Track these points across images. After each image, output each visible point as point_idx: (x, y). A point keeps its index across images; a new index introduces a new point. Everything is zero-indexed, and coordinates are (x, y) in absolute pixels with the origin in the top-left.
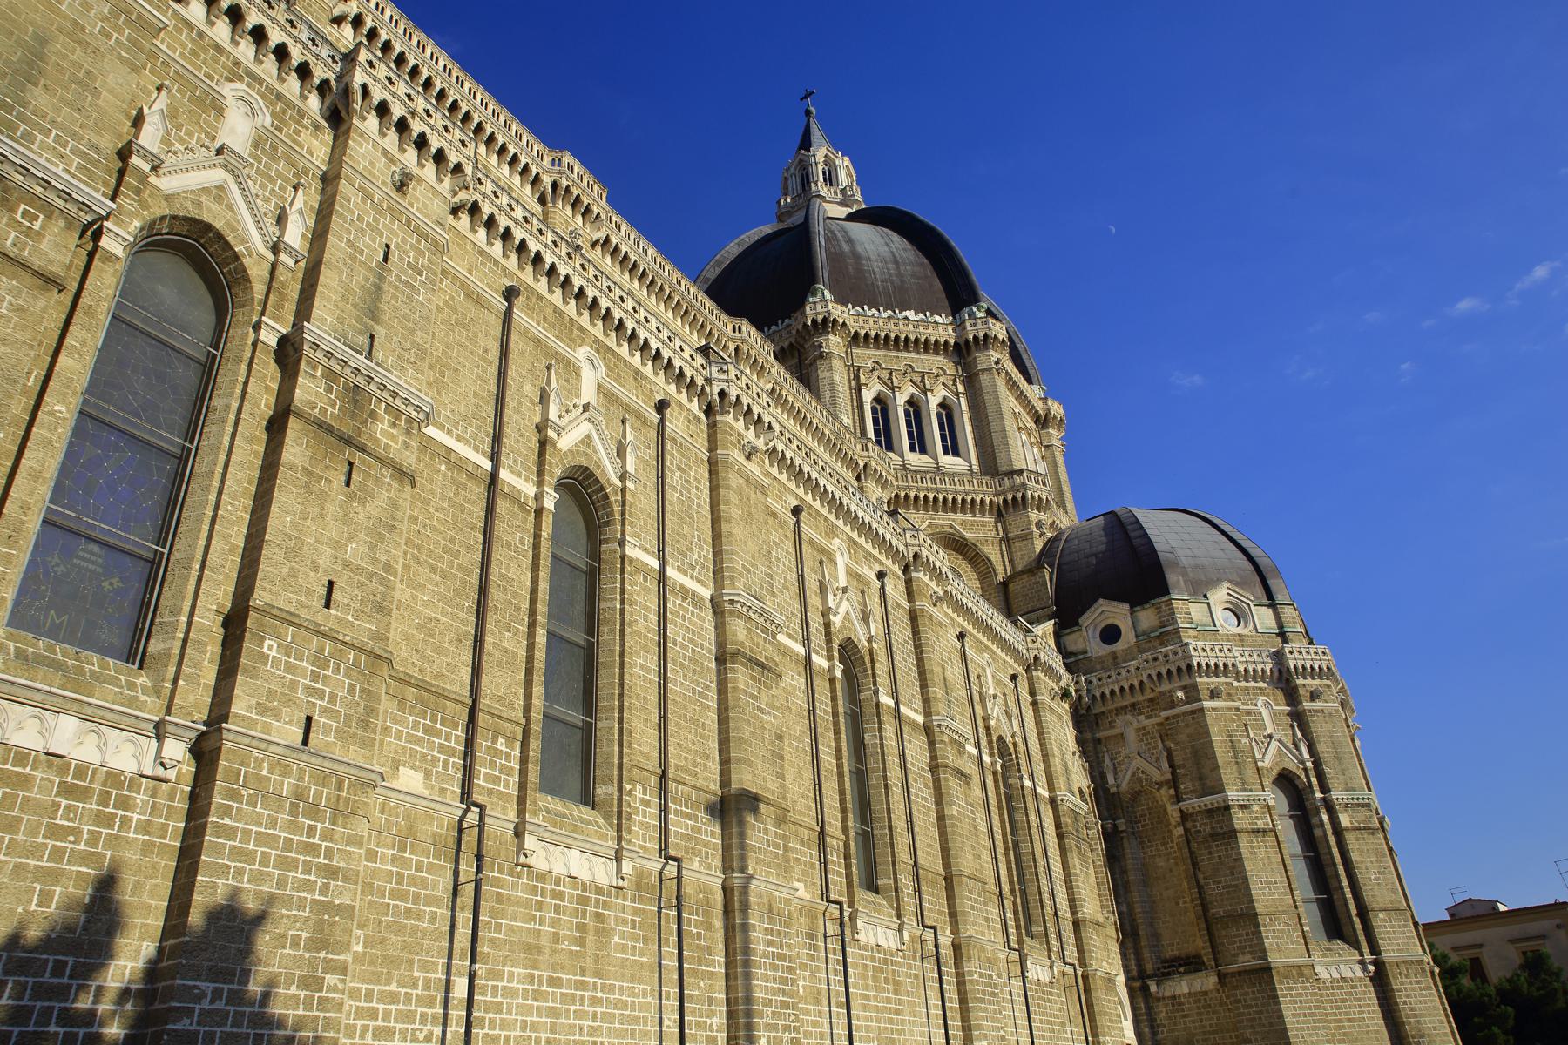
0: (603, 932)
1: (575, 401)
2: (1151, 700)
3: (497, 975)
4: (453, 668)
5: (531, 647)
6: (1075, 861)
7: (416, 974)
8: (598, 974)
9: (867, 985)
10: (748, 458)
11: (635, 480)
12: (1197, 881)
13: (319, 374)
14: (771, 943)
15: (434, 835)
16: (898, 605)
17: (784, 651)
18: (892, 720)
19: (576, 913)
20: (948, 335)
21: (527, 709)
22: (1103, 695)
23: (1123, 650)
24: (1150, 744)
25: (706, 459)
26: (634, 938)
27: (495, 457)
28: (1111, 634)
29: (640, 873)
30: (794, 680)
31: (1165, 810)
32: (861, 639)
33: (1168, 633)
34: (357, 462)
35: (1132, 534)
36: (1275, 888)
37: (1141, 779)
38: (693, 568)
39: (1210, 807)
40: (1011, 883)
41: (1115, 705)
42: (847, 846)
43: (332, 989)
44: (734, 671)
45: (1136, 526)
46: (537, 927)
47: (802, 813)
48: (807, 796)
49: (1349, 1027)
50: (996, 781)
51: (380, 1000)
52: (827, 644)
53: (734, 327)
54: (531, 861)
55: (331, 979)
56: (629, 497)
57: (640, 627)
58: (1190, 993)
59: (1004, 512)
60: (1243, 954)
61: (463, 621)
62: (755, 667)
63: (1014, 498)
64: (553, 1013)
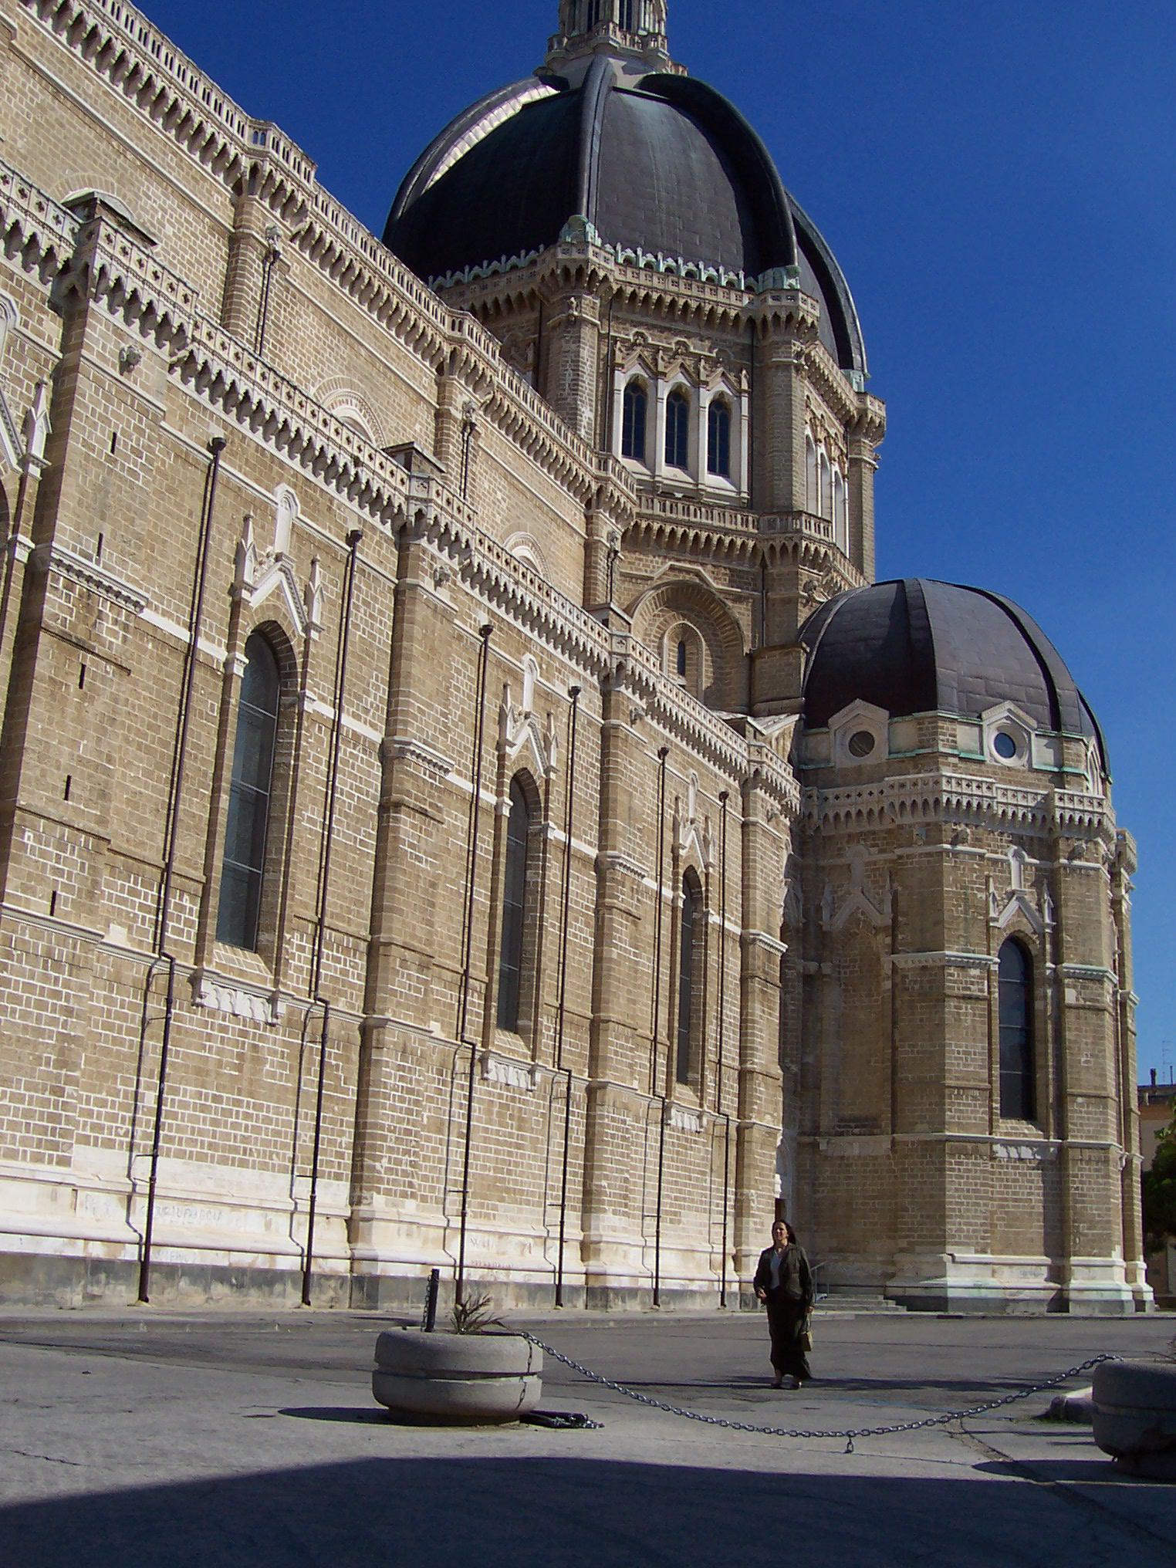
0: (259, 1061)
1: (269, 549)
2: (889, 832)
3: (176, 1091)
4: (151, 836)
5: (214, 811)
6: (757, 1009)
7: (119, 1087)
8: (251, 1095)
9: (491, 1120)
10: (438, 583)
11: (319, 630)
12: (893, 1041)
13: (60, 586)
14: (402, 1078)
15: (135, 979)
16: (590, 723)
17: (449, 790)
18: (560, 855)
19: (236, 1044)
20: (736, 303)
21: (208, 869)
22: (837, 816)
23: (871, 766)
24: (877, 882)
25: (393, 586)
26: (282, 1066)
27: (194, 627)
28: (862, 742)
29: (291, 1012)
30: (457, 819)
31: (879, 959)
32: (538, 772)
33: (925, 758)
34: (88, 663)
35: (915, 622)
36: (973, 1060)
37: (859, 919)
38: (367, 711)
39: (924, 964)
40: (670, 1028)
41: (848, 831)
42: (488, 986)
43: (71, 1096)
44: (397, 820)
45: (921, 611)
46: (207, 1054)
47: (448, 957)
48: (455, 939)
49: (1013, 1206)
50: (674, 918)
51: (95, 1105)
52: (498, 778)
53: (453, 322)
54: (204, 1002)
55: (68, 1089)
56: (312, 649)
57: (310, 782)
58: (859, 1157)
59: (768, 563)
60: (922, 1123)
61: (161, 792)
62: (417, 815)
63: (784, 548)
64: (215, 1123)
